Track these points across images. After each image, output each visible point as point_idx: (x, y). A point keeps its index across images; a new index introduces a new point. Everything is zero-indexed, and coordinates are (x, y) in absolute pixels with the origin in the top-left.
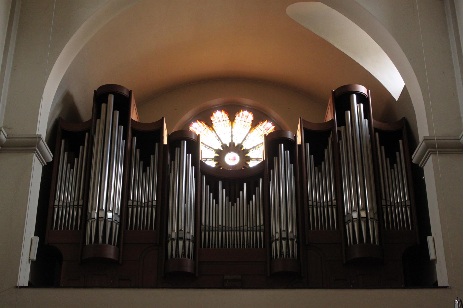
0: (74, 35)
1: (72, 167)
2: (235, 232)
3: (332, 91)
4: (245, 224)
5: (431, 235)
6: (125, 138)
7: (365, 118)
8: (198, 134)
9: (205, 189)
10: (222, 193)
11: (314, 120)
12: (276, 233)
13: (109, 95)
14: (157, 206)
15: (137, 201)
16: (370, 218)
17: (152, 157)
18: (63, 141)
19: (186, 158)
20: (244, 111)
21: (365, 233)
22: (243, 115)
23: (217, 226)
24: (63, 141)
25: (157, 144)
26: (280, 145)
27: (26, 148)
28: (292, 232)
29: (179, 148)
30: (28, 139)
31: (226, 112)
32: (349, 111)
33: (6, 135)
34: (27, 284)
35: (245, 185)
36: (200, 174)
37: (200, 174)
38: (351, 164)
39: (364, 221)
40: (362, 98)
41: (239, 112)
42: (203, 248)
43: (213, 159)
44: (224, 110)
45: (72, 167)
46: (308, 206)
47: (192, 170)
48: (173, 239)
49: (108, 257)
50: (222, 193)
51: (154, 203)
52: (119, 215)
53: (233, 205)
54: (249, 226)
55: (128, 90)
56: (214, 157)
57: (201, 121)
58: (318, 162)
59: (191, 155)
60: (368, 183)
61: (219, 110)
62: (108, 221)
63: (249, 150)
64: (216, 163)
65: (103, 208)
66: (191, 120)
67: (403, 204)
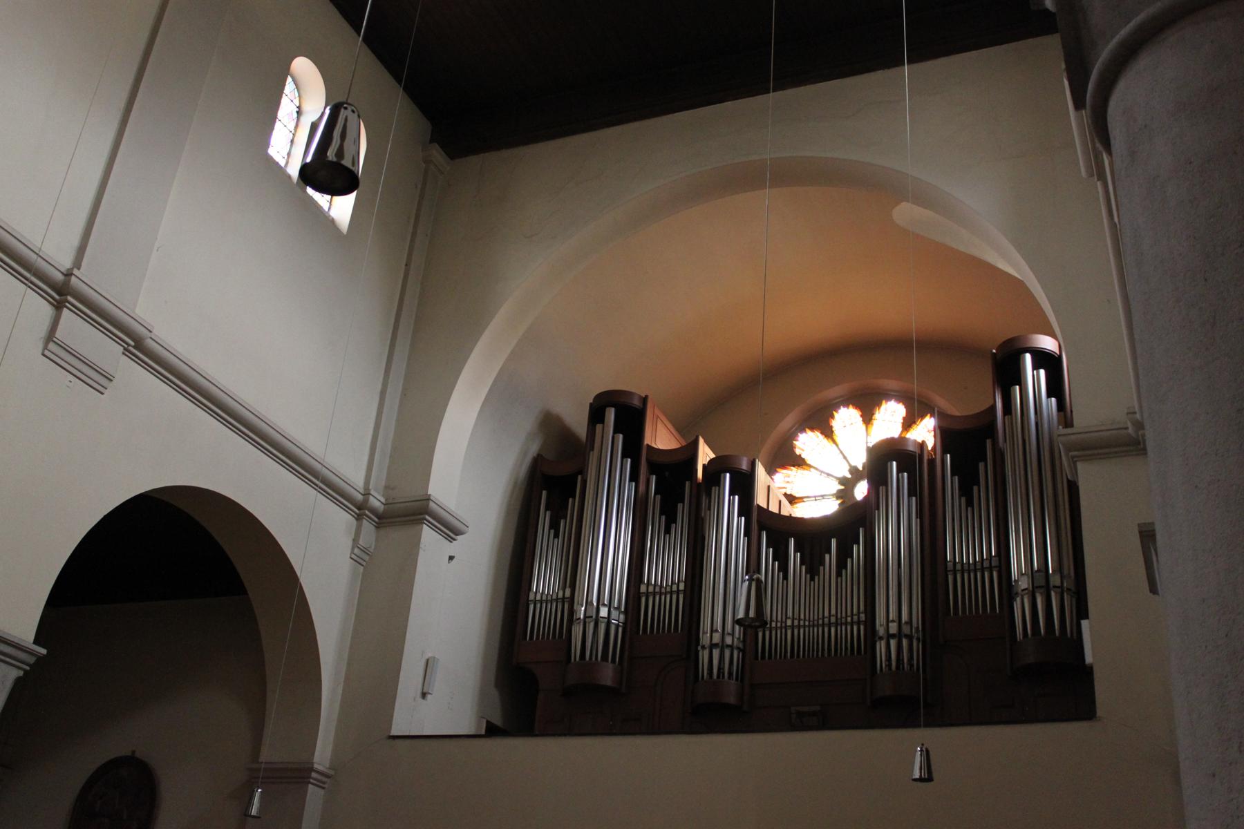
0: (492, 323)
1: (556, 536)
2: (816, 629)
3: (992, 351)
4: (833, 612)
5: (1087, 617)
6: (634, 477)
7: (1049, 395)
8: (429, 493)
9: (767, 554)
10: (794, 557)
11: (963, 408)
12: (881, 625)
13: (607, 409)
14: (685, 591)
15: (661, 586)
16: (1067, 589)
17: (680, 506)
18: (544, 493)
19: (729, 503)
20: (839, 411)
21: (1043, 616)
22: (886, 410)
23: (784, 620)
24: (544, 493)
25: (688, 483)
26: (889, 464)
27: (412, 518)
28: (910, 622)
29: (717, 488)
30: (418, 503)
31: (857, 407)
32: (1018, 387)
33: (383, 500)
34: (483, 732)
35: (834, 542)
36: (755, 526)
37: (755, 526)
38: (1021, 487)
39: (1041, 594)
40: (1045, 360)
41: (879, 405)
42: (760, 659)
43: (833, 495)
44: (853, 405)
45: (556, 536)
46: (946, 571)
47: (739, 523)
48: (881, 638)
49: (603, 683)
50: (794, 557)
51: (682, 587)
52: (623, 610)
53: (812, 579)
54: (839, 616)
55: (640, 397)
56: (835, 492)
57: (812, 429)
58: (966, 490)
59: (737, 497)
60: (1053, 522)
61: (844, 406)
62: (613, 623)
63: (837, 478)
64: (839, 502)
65: (592, 600)
66: (796, 429)
67: (979, 566)
